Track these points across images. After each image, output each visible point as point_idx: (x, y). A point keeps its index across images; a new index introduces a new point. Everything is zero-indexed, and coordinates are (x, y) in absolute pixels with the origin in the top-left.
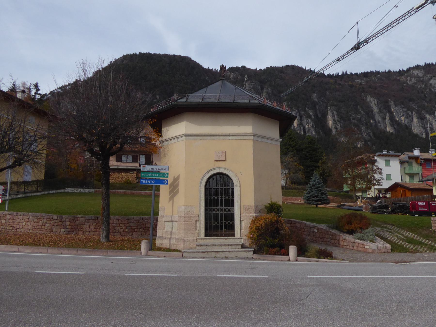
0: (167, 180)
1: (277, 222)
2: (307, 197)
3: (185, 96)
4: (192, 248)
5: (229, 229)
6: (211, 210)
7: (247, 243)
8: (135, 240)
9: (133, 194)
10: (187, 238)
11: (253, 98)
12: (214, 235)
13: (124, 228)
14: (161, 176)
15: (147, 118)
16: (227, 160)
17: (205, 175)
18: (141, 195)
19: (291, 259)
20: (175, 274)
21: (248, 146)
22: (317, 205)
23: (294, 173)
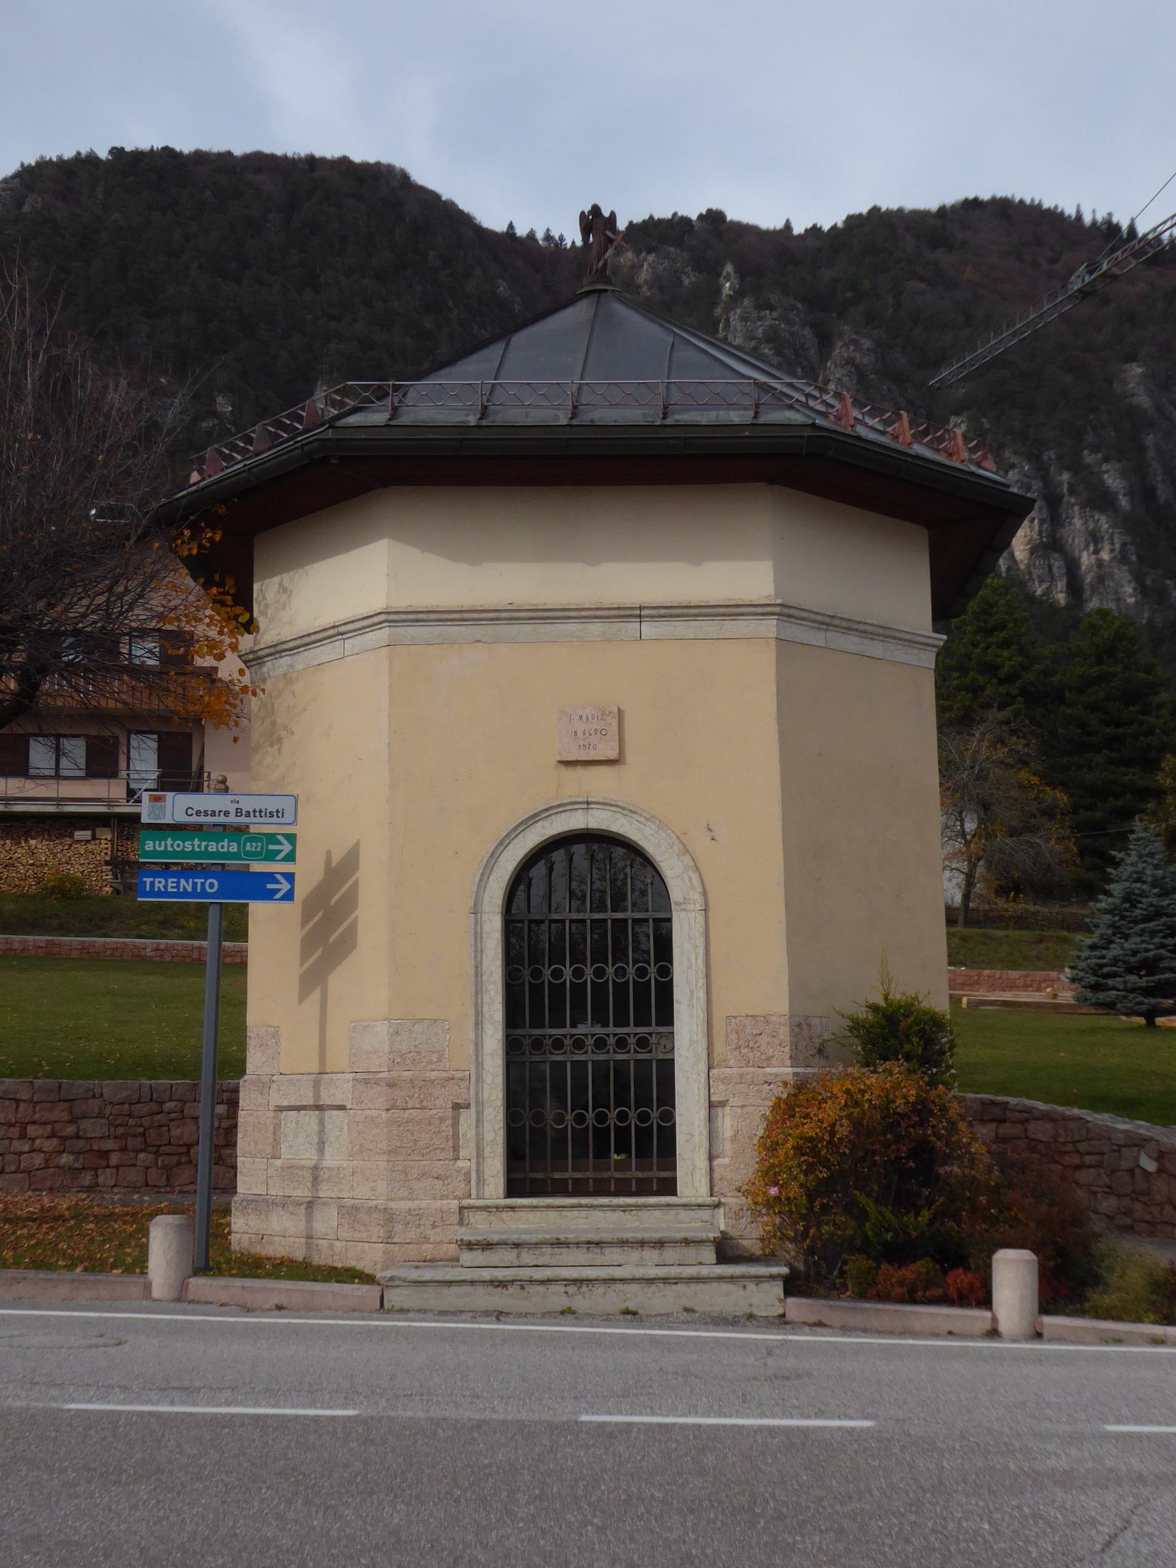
0: (290, 877)
1: (922, 1110)
2: (1095, 970)
3: (382, 394)
4: (432, 1261)
5: (643, 1152)
6: (537, 1044)
7: (750, 1235)
8: (111, 1216)
9: (91, 959)
10: (404, 1205)
11: (779, 396)
12: (559, 1189)
13: (50, 1145)
14: (255, 856)
15: (168, 521)
16: (629, 756)
17: (504, 843)
18: (138, 960)
19: (1004, 1326)
20: (344, 1407)
21: (743, 681)
22: (1151, 1015)
23: (1012, 833)
